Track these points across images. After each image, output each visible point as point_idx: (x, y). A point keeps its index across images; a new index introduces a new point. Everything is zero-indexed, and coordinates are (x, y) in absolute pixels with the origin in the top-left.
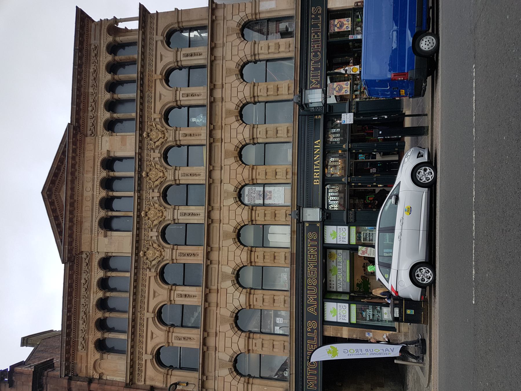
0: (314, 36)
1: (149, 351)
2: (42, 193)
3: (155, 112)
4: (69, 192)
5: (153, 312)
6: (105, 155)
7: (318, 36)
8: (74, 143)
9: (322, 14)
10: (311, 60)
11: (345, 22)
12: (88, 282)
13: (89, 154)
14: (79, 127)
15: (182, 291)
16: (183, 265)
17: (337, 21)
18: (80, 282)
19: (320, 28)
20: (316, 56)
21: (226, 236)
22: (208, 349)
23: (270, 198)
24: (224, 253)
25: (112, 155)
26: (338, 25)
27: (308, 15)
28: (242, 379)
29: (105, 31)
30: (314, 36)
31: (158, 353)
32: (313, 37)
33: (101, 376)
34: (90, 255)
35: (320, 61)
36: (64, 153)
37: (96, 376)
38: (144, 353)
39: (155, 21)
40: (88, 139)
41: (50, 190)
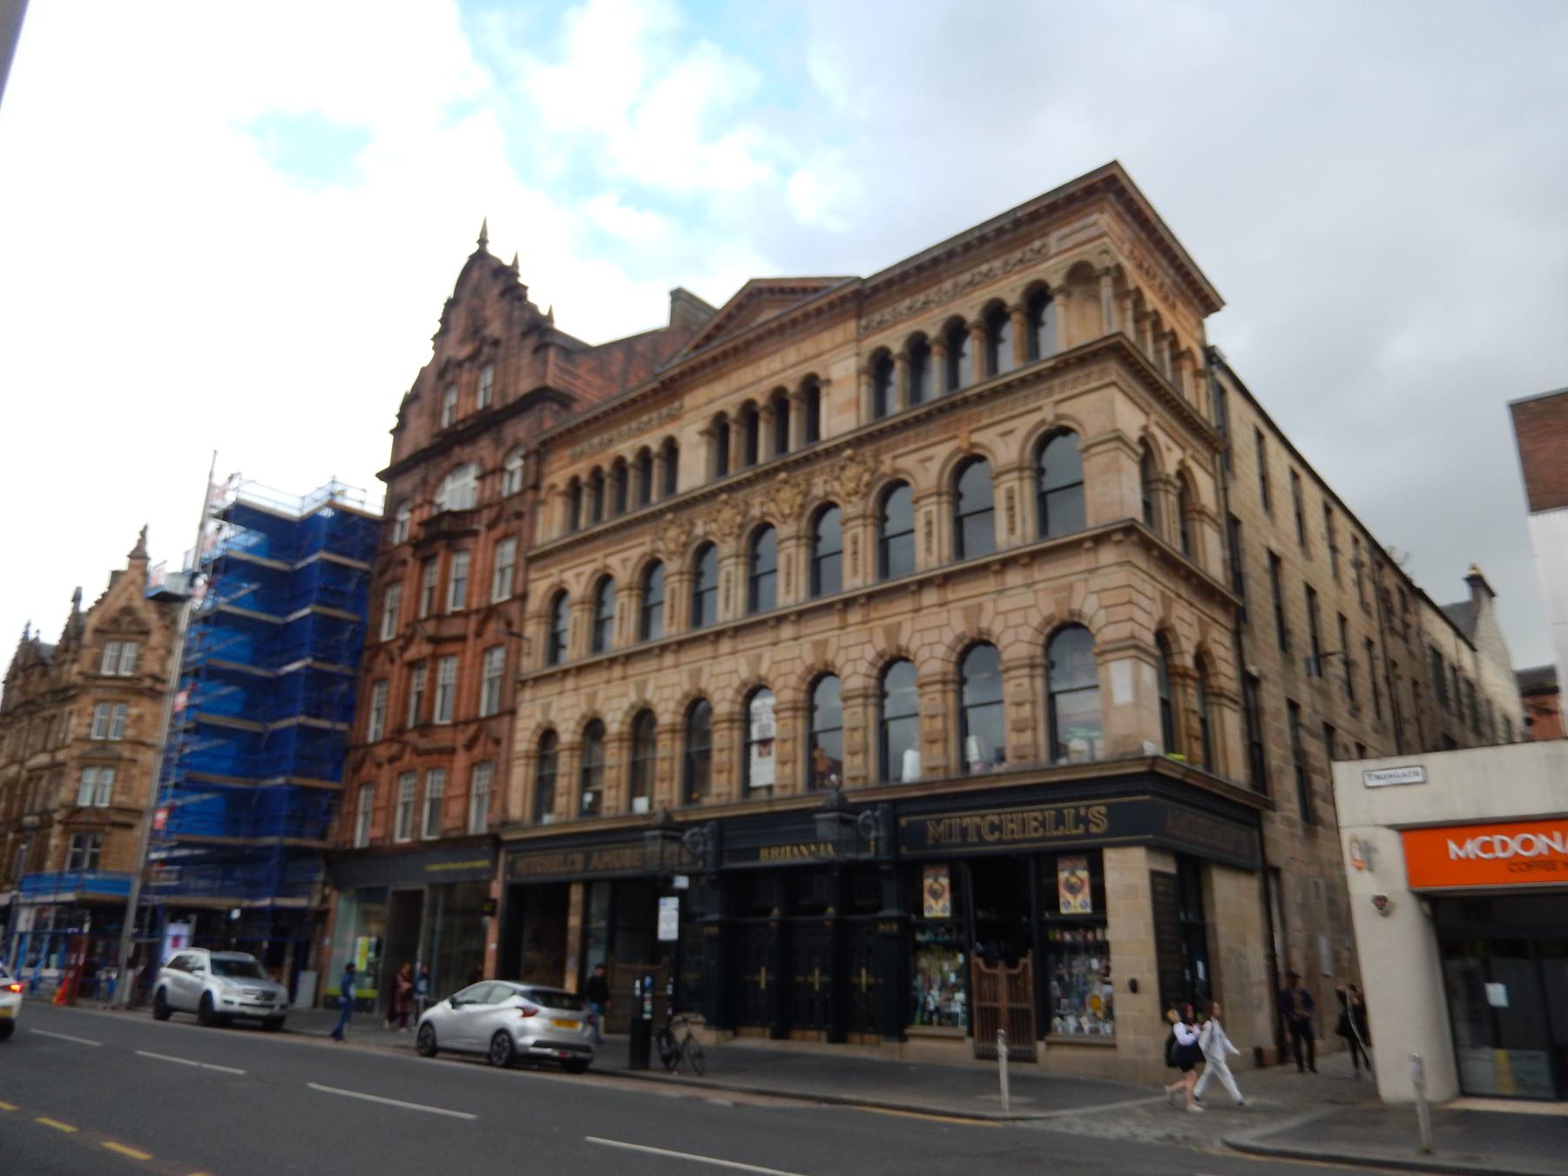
0: (1036, 819)
1: (1065, 408)
2: (752, 282)
3: (1058, 403)
4: (773, 325)
5: (1059, 417)
6: (822, 376)
7: (1036, 829)
8: (831, 305)
9: (1088, 835)
10: (983, 817)
11: (1080, 898)
12: (989, 277)
13: (808, 347)
14: (867, 297)
15: (574, 634)
16: (1075, 479)
17: (945, 881)
18: (979, 265)
19: (1055, 833)
20: (994, 828)
21: (973, 613)
22: (914, 593)
23: (761, 754)
24: (1024, 598)
25: (823, 391)
26: (1073, 880)
27: (1081, 798)
28: (1039, 651)
29: (1072, 261)
30: (1036, 819)
31: (1065, 431)
32: (1033, 815)
33: (544, 502)
34: (674, 417)
35: (982, 842)
36: (816, 290)
37: (542, 495)
38: (1057, 397)
39: (912, 447)
40: (852, 326)
41: (760, 291)
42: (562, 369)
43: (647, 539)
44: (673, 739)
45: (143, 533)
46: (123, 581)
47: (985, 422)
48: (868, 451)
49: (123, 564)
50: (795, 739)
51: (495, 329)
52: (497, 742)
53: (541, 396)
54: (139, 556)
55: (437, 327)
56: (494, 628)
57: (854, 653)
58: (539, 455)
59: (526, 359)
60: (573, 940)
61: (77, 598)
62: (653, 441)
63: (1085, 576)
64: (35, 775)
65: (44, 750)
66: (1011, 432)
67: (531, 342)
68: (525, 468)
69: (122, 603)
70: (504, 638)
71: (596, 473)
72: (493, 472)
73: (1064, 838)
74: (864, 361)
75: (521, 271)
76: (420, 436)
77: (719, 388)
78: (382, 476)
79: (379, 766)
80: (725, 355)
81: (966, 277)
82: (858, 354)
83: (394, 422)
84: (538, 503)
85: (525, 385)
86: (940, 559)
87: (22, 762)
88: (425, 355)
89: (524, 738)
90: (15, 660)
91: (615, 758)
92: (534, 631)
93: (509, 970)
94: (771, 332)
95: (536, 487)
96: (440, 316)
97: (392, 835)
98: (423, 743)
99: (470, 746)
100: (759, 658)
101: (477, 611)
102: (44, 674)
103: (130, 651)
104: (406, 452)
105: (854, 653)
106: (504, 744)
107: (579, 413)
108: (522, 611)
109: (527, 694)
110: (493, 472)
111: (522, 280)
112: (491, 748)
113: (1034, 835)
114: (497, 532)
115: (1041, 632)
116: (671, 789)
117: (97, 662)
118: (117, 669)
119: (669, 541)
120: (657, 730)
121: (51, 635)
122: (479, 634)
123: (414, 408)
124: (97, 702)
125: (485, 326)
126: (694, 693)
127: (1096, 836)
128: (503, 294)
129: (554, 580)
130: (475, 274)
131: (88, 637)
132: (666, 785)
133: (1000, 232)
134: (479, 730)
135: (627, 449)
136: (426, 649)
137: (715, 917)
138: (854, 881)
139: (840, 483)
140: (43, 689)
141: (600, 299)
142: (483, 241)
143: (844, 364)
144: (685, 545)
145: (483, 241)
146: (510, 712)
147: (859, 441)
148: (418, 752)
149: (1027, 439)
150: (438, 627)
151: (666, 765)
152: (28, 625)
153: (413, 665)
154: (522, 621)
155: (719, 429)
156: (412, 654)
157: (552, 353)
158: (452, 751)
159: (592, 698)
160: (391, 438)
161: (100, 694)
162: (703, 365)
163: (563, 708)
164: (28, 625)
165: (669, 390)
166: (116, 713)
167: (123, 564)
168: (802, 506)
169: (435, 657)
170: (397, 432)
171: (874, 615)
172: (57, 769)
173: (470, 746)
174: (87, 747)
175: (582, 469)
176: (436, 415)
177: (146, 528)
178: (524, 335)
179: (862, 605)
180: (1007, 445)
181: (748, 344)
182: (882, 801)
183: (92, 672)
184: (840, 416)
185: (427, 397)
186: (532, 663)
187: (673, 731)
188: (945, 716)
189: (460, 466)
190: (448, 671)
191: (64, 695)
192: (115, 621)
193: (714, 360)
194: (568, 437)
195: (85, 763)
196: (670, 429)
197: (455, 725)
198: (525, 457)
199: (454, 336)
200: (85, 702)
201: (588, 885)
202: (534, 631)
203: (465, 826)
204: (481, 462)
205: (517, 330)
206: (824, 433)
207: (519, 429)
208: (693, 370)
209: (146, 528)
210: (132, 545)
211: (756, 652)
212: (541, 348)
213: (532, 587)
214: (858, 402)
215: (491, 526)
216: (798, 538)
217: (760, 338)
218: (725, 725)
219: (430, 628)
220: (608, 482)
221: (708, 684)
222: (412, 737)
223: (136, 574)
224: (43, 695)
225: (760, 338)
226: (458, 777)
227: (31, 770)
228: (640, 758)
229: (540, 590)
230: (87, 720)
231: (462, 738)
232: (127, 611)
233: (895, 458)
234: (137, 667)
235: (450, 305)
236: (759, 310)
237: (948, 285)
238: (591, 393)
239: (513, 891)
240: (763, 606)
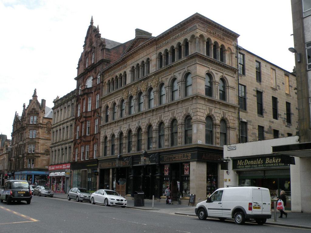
34: (126, 67)
42: (107, 54)
43: (121, 95)
44: (126, 139)
45: (35, 91)
46: (32, 102)
47: (176, 71)
48: (157, 76)
49: (32, 98)
50: (145, 139)
51: (94, 44)
52: (97, 139)
53: (102, 62)
54: (35, 96)
55: (84, 43)
56: (96, 115)
57: (154, 121)
58: (103, 75)
59: (100, 52)
60: (111, 180)
61: (24, 106)
62: (122, 72)
63: (190, 106)
64: (20, 146)
65: (21, 141)
66: (181, 73)
67: (101, 48)
68: (100, 77)
69: (33, 107)
70: (98, 117)
71: (173, 49)
72: (95, 79)
73: (182, 160)
74: (157, 55)
75: (99, 28)
76: (82, 71)
77: (133, 60)
78: (76, 79)
79: (78, 144)
80: (133, 53)
81: (174, 37)
82: (156, 54)
83: (77, 66)
84: (103, 86)
85: (100, 58)
86: (182, 97)
87: (18, 143)
88: (82, 50)
89: (102, 139)
90: (14, 120)
91: (144, 137)
92: (103, 115)
93: (101, 187)
94: (141, 48)
95: (102, 82)
96: (84, 41)
97: (81, 159)
98: (84, 139)
99: (93, 140)
100: (139, 122)
101: (93, 111)
102: (20, 124)
103: (35, 118)
104: (80, 73)
105: (154, 121)
106: (99, 140)
107: (112, 64)
108: (101, 110)
109: (102, 129)
110: (95, 79)
111: (100, 33)
112: (96, 141)
113: (180, 159)
114: (96, 93)
115: (158, 124)
116: (145, 146)
117: (29, 121)
118: (33, 122)
119: (124, 95)
120: (192, 121)
121: (20, 114)
122: (94, 116)
123: (81, 63)
124: (30, 130)
125: (93, 43)
126: (173, 118)
127: (189, 159)
128: (95, 36)
129: (172, 75)
130: (90, 32)
131: (26, 115)
132: (167, 141)
133: (179, 27)
134: (94, 137)
135: (118, 74)
136: (84, 119)
137: (132, 176)
138: (153, 168)
139: (152, 83)
140: (20, 127)
141: (117, 33)
142: (92, 23)
143: (154, 56)
144: (127, 96)
145: (92, 23)
146: (99, 133)
147: (156, 74)
148: (84, 142)
149: (183, 75)
150: (86, 114)
151: (144, 142)
152: (16, 112)
153: (82, 123)
154: (101, 113)
155: (133, 70)
156: (81, 120)
157: (104, 50)
158: (90, 141)
159: (160, 117)
160: (77, 70)
161: (30, 128)
162: (129, 55)
163: (107, 132)
164: (16, 112)
165: (124, 61)
166: (34, 132)
167: (32, 98)
168: (147, 88)
169: (86, 121)
170: (78, 68)
171: (158, 113)
172: (24, 145)
173: (93, 140)
174: (29, 140)
175: (110, 78)
176: (85, 65)
177: (35, 89)
178: (100, 46)
179: (144, 114)
180: (180, 76)
181: (137, 51)
182: (157, 152)
183: (28, 123)
184: (153, 69)
185: (83, 60)
186: (103, 122)
187: (126, 137)
188: (182, 133)
189: (89, 77)
190: (88, 124)
191: (23, 128)
192: (31, 112)
193: (131, 54)
194: (110, 69)
195: (29, 143)
196: (125, 70)
197: (90, 135)
198: (100, 75)
199: (87, 45)
200: (27, 130)
201: (113, 169)
202: (103, 115)
203: (93, 157)
204: (93, 77)
205: (99, 45)
206: (127, 83)
207: (100, 69)
208: (128, 57)
209: (35, 89)
210: (33, 94)
211: (173, 111)
212: (102, 50)
213: (102, 105)
214: (156, 65)
215: (95, 91)
216: (146, 95)
217: (139, 50)
218: (134, 136)
219: (84, 115)
220: (145, 65)
221: (163, 119)
222: (83, 139)
223: (35, 100)
224: (20, 128)
225: (139, 50)
226: (91, 147)
227: (20, 145)
228: (131, 140)
229: (103, 106)
230: (28, 134)
231: (92, 138)
232: (34, 109)
233: (162, 78)
234: (37, 122)
235: (86, 38)
236: (139, 42)
237: (171, 38)
238: (115, 58)
239: (101, 170)
240: (150, 108)
